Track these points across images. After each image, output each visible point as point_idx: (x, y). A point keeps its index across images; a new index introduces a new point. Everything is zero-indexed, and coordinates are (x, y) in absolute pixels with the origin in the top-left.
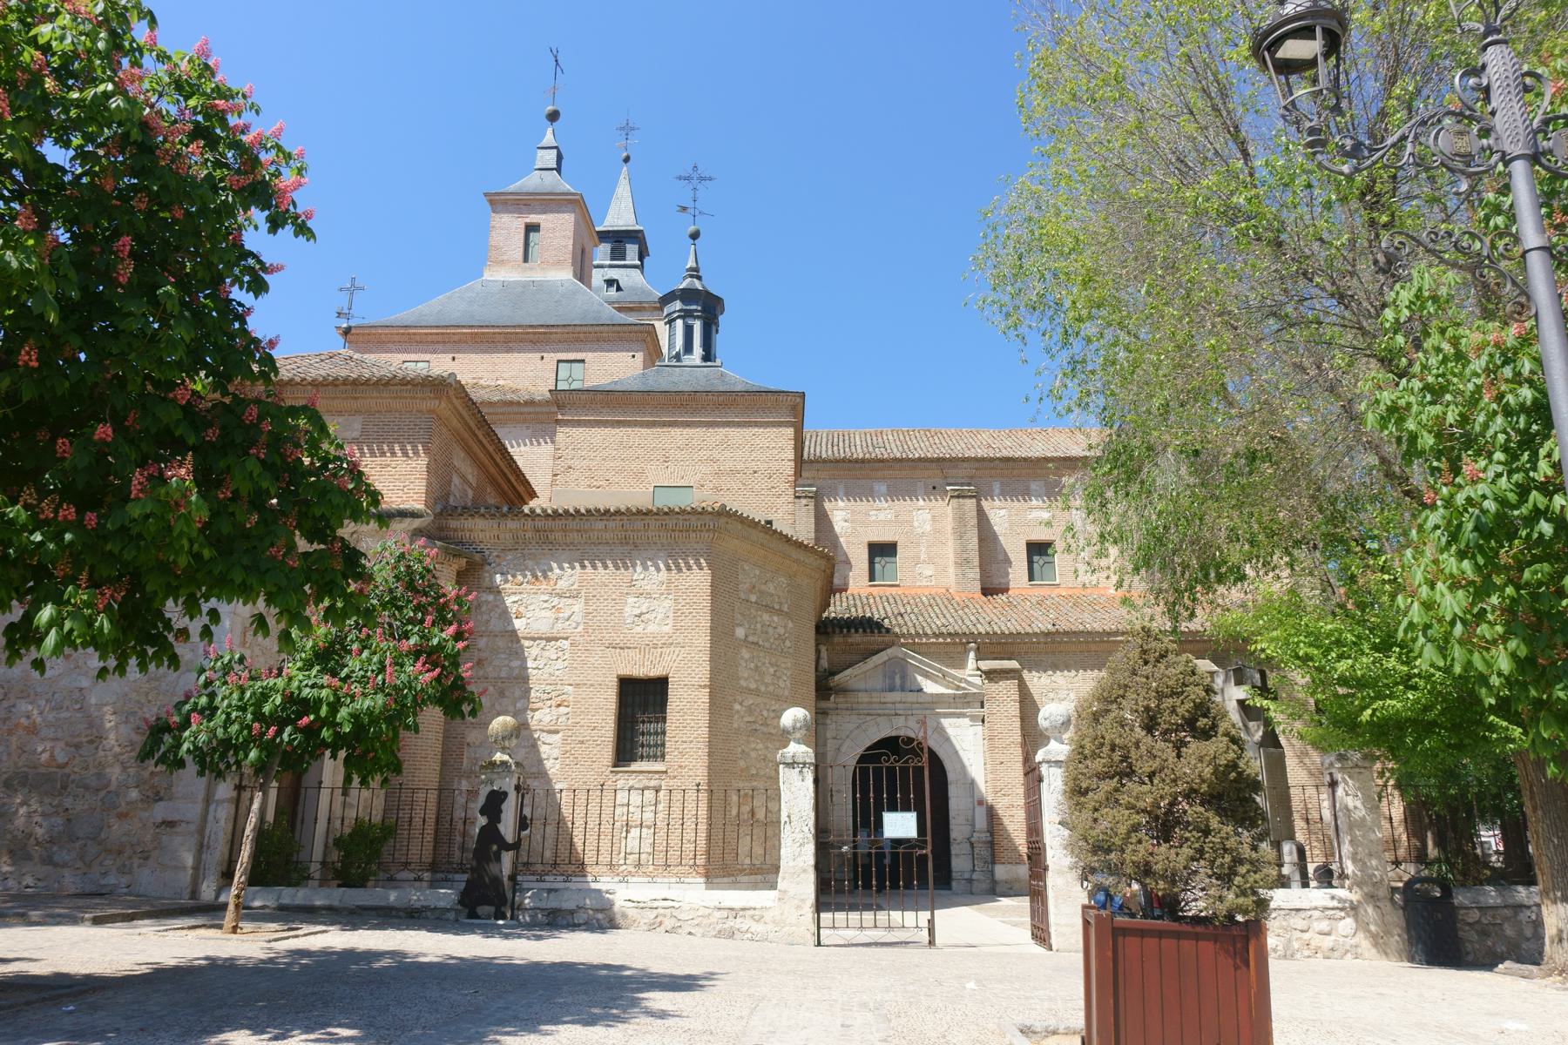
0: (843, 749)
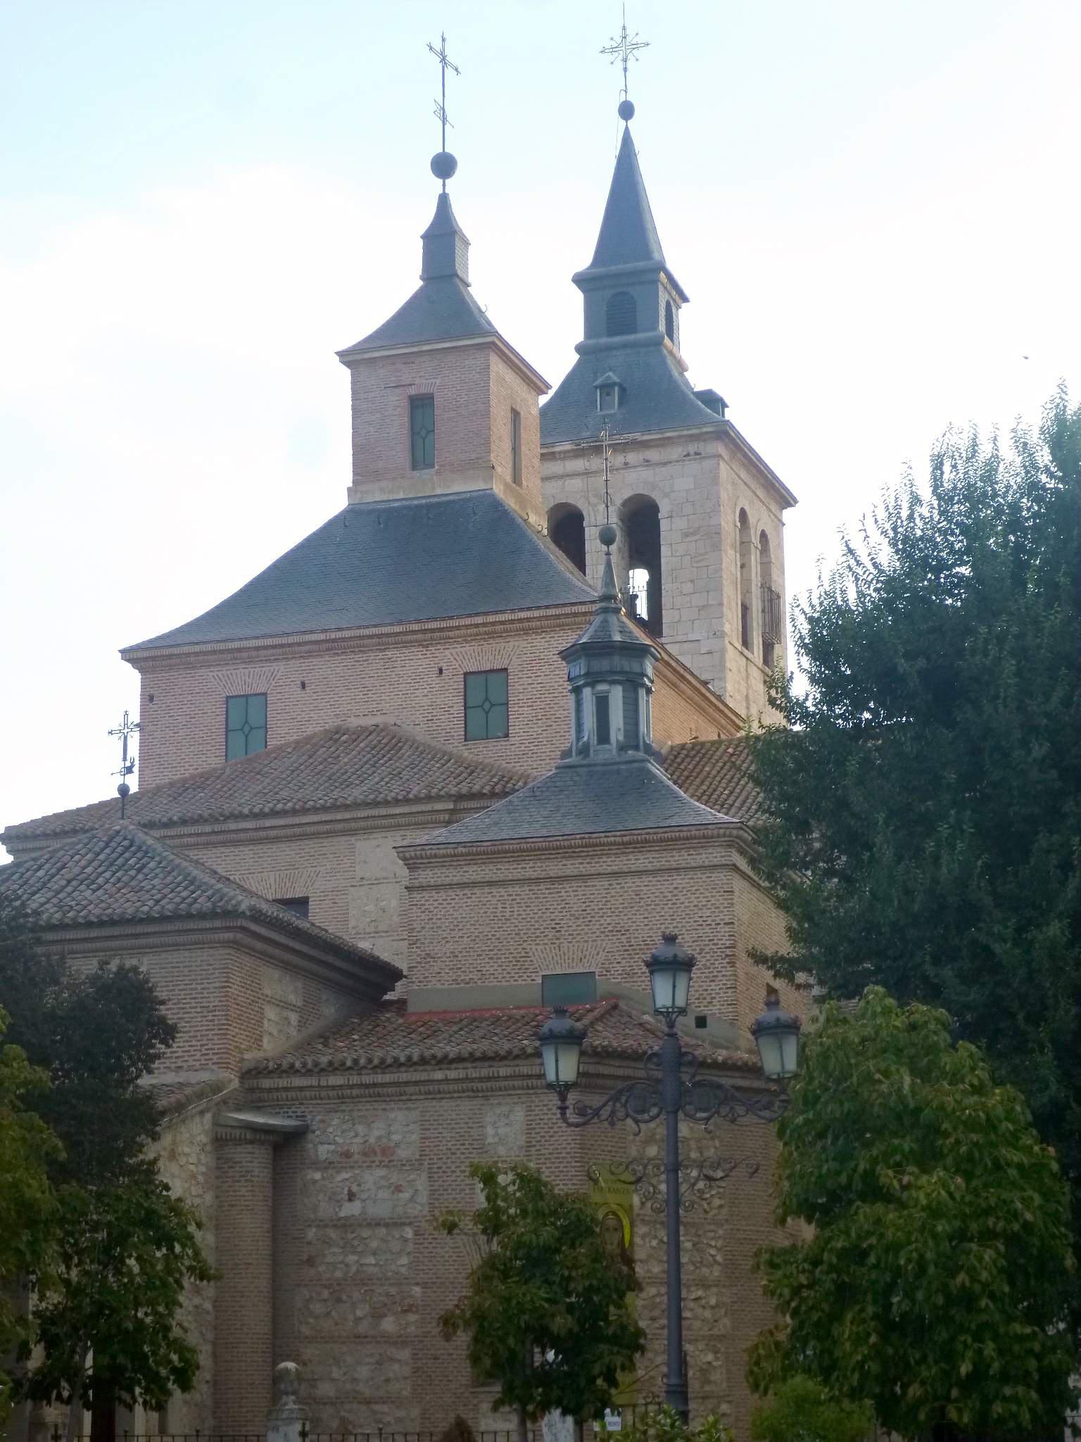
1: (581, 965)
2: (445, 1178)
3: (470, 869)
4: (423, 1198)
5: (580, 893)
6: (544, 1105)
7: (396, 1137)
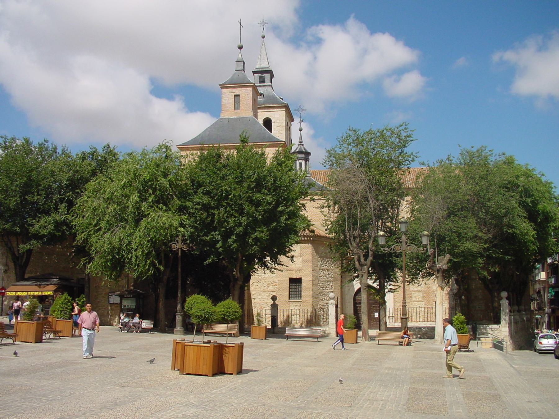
0: (350, 290)
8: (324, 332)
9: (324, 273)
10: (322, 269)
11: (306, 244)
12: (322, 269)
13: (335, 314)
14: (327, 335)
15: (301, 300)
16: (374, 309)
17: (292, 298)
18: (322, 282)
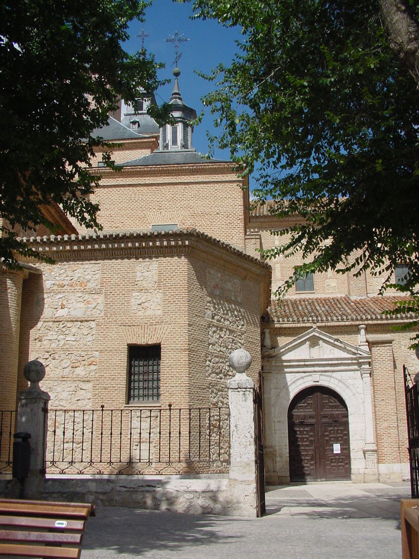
0: (281, 395)
1: (170, 221)
2: (114, 298)
3: (120, 179)
4: (101, 307)
5: (171, 191)
6: (169, 262)
7: (88, 277)
8: (213, 496)
9: (220, 337)
10: (217, 327)
11: (172, 256)
12: (217, 327)
13: (253, 425)
14: (224, 508)
15: (159, 403)
16: (331, 436)
17: (136, 399)
18: (217, 359)
